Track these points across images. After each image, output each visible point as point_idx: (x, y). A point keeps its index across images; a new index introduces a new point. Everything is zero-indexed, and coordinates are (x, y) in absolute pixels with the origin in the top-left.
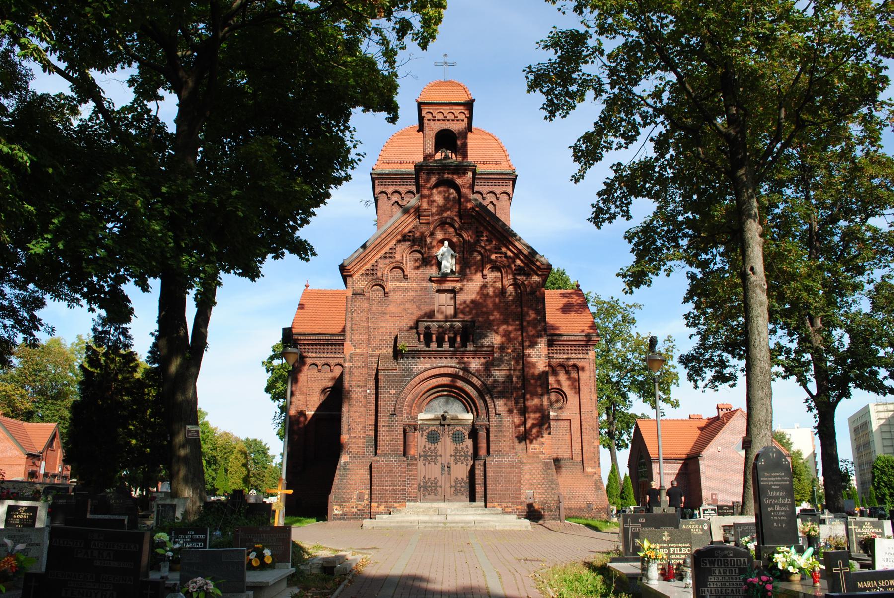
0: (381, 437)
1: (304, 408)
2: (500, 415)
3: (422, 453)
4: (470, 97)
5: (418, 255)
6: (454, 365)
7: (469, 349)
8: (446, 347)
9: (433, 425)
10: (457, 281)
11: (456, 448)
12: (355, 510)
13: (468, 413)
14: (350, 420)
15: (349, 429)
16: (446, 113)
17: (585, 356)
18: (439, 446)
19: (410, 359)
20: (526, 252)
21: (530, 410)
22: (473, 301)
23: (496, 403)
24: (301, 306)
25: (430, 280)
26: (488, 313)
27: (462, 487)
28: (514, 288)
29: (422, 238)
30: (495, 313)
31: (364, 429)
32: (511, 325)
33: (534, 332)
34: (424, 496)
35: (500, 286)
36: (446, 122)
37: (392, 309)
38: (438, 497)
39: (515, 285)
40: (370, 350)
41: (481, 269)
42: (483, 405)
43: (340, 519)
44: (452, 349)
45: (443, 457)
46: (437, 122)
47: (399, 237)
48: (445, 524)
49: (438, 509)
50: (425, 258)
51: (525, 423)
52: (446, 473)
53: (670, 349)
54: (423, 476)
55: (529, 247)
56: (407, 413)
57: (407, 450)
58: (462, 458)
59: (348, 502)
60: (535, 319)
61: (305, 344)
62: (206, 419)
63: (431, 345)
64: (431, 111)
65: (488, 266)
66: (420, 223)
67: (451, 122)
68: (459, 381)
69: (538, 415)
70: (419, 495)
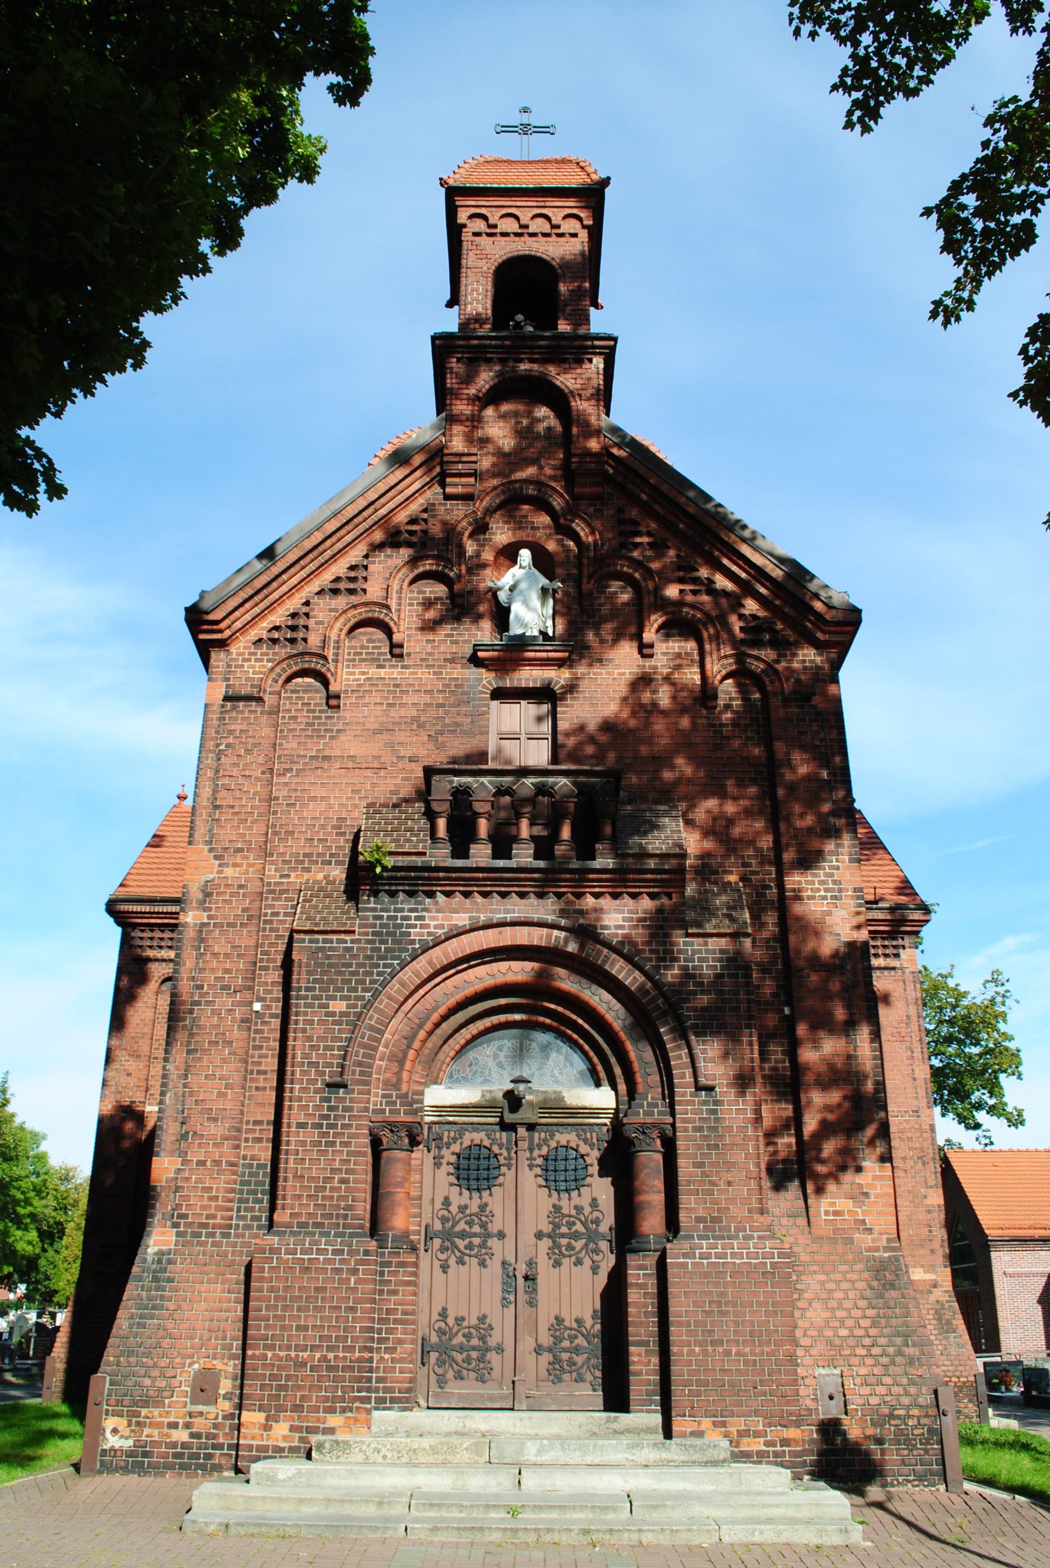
0: (289, 1164)
1: (138, 1097)
2: (710, 1089)
3: (438, 1226)
4: (594, 177)
5: (439, 590)
6: (550, 918)
7: (598, 863)
8: (524, 856)
9: (475, 1127)
10: (560, 663)
11: (557, 1208)
12: (181, 1435)
13: (598, 1084)
14: (190, 1102)
15: (184, 1136)
16: (525, 216)
17: (892, 962)
18: (497, 1200)
19: (401, 896)
20: (777, 573)
21: (809, 1078)
22: (608, 726)
23: (698, 1049)
24: (157, 841)
25: (475, 660)
26: (663, 760)
27: (577, 1350)
28: (739, 685)
29: (450, 540)
30: (680, 761)
31: (235, 1136)
32: (735, 799)
33: (809, 820)
34: (442, 1382)
35: (697, 678)
36: (526, 238)
37: (349, 745)
38: (489, 1389)
39: (740, 674)
40: (271, 871)
41: (633, 629)
42: (649, 1055)
43: (125, 1470)
44: (541, 864)
45: (510, 1240)
46: (499, 238)
47: (378, 536)
48: (513, 1512)
49: (488, 1438)
50: (461, 595)
51: (796, 1121)
52: (522, 1297)
53: (999, 999)
54: (437, 1309)
55: (783, 560)
56: (387, 1083)
57: (381, 1213)
58: (579, 1244)
59: (160, 1404)
60: (809, 778)
61: (152, 927)
62: (44, 1147)
63: (474, 849)
64: (483, 211)
65: (656, 620)
66: (447, 497)
67: (540, 238)
68: (561, 972)
69: (835, 1096)
70: (421, 1381)
